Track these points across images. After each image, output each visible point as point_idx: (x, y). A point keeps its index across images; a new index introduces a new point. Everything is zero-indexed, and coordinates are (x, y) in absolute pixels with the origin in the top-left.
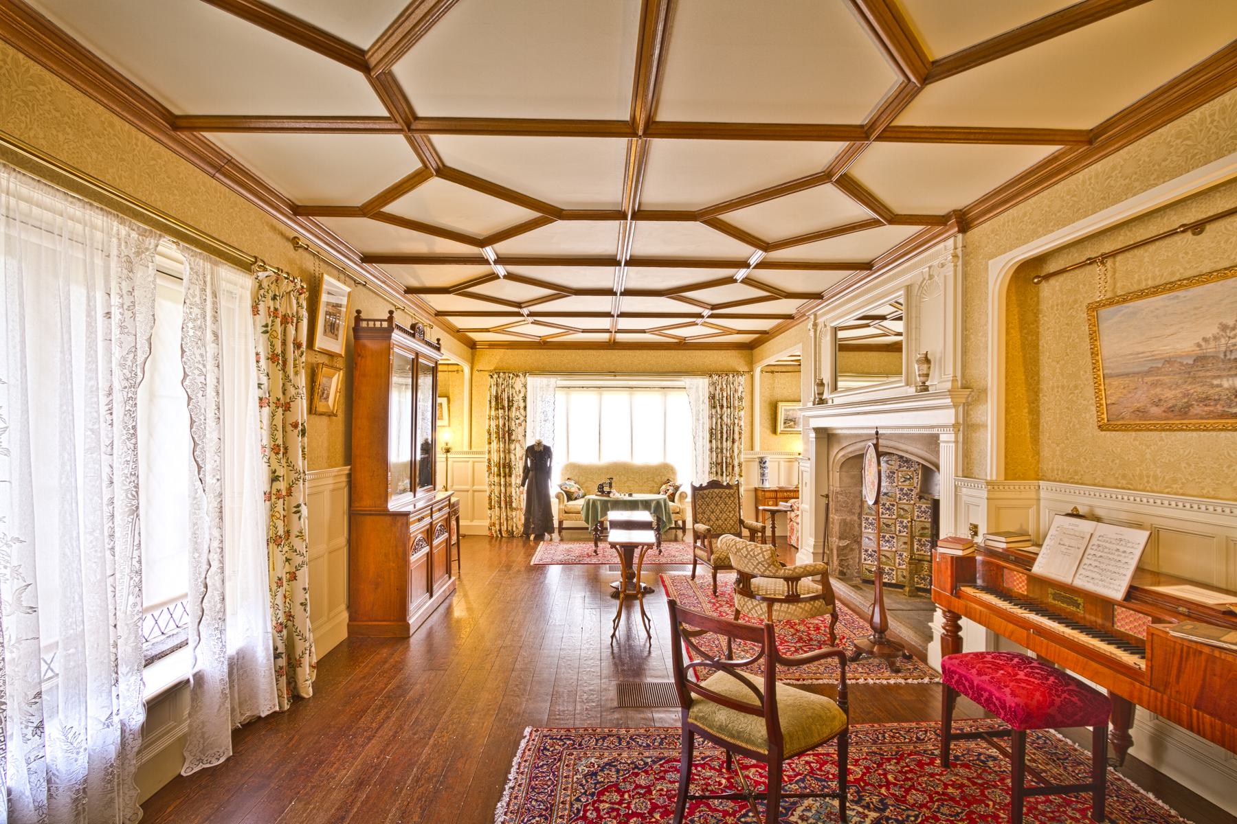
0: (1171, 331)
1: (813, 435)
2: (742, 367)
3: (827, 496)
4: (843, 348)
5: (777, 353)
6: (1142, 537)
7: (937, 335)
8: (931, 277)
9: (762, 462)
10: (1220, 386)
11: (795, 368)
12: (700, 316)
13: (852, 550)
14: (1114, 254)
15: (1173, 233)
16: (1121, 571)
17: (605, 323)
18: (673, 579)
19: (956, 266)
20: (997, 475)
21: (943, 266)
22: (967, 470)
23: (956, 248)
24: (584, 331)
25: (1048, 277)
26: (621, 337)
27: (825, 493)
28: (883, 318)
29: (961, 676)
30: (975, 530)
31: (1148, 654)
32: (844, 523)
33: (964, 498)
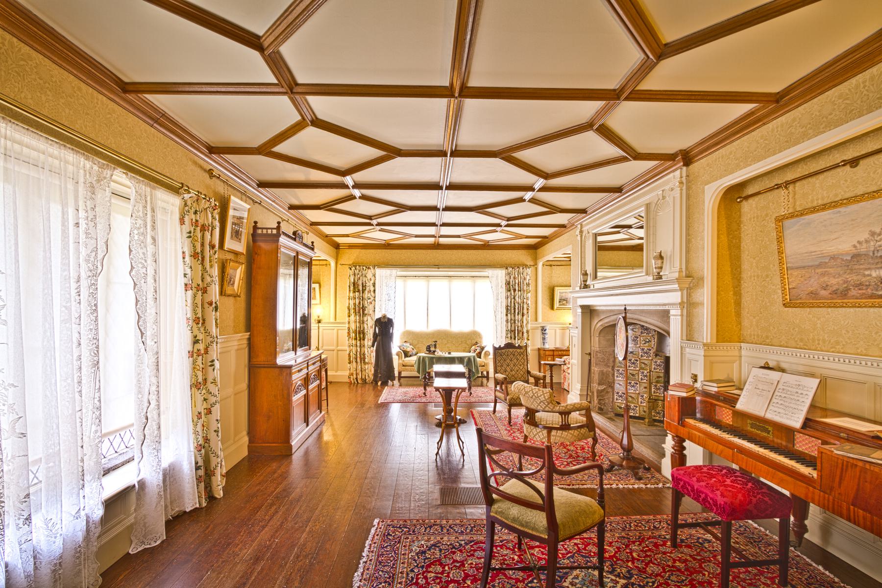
0: (835, 237)
1: (579, 310)
2: (529, 262)
3: (590, 354)
4: (601, 248)
5: (554, 252)
6: (814, 383)
7: (668, 239)
8: (664, 197)
9: (543, 330)
10: (870, 275)
11: (567, 262)
12: (499, 225)
13: (607, 392)
14: (794, 181)
15: (837, 166)
16: (800, 407)
17: (431, 230)
18: (480, 413)
19: (681, 190)
20: (711, 339)
21: (672, 189)
22: (689, 335)
23: (681, 177)
24: (417, 236)
25: (747, 197)
26: (443, 241)
27: (588, 352)
28: (630, 227)
29: (685, 482)
30: (695, 378)
31: (819, 467)
32: (602, 373)
33: (687, 355)
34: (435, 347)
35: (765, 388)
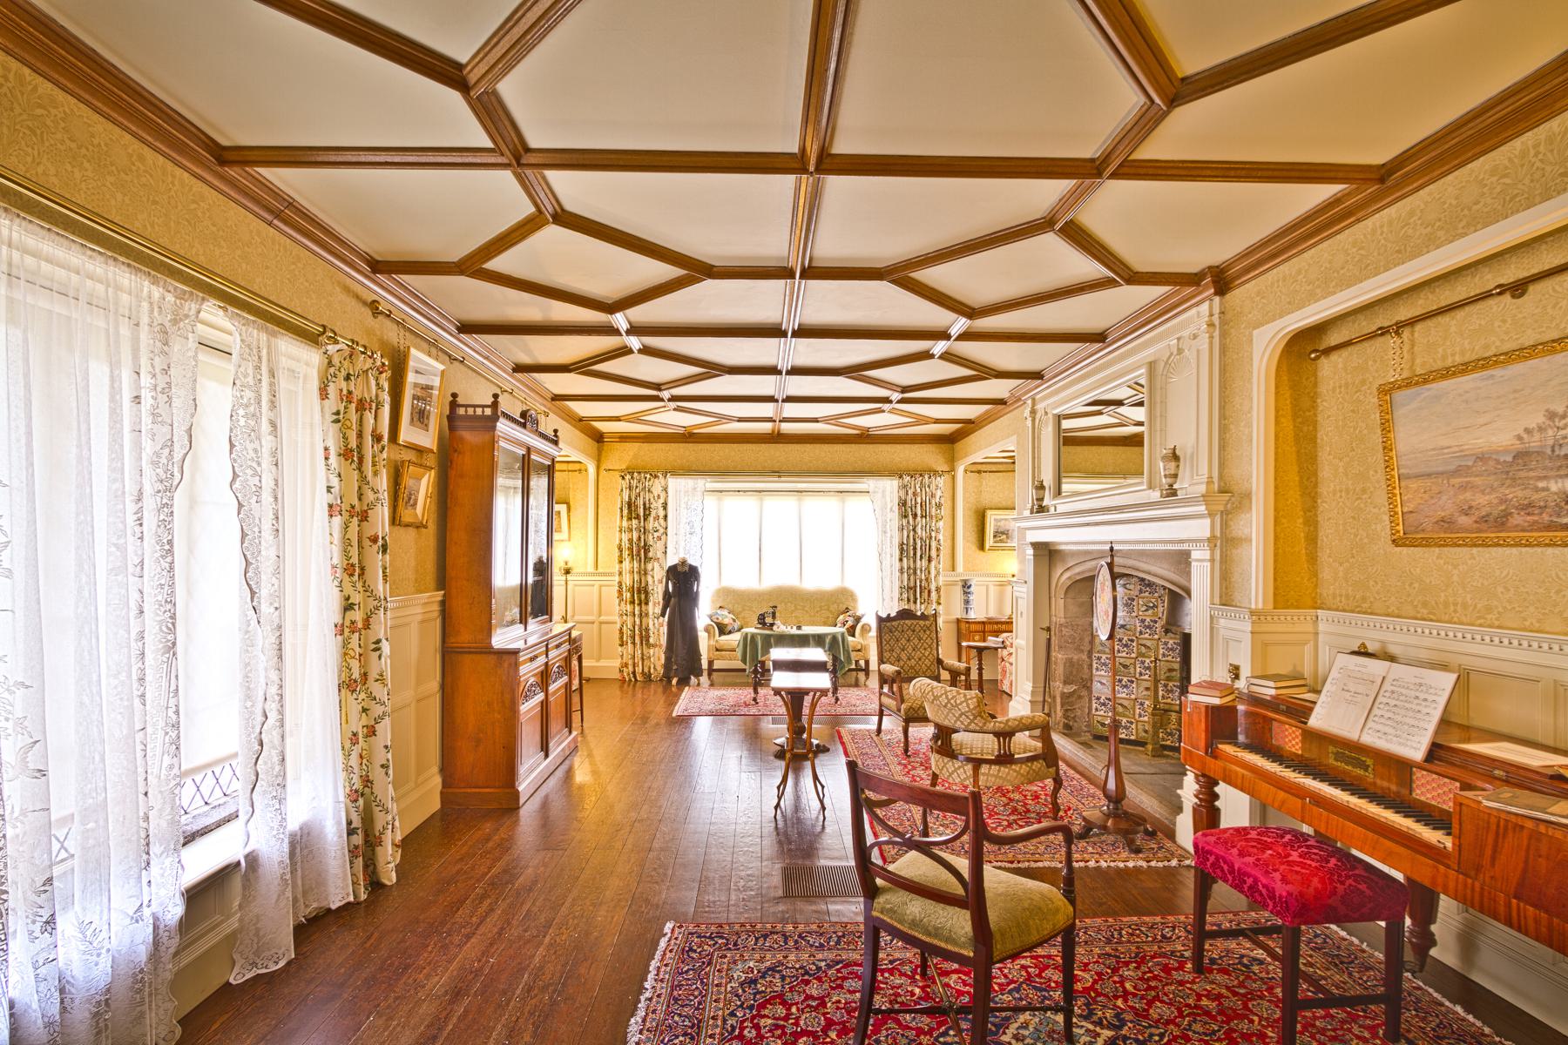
1: (1030, 551)
2: (941, 466)
3: (1049, 629)
4: (1068, 441)
5: (985, 447)
6: (1447, 680)
7: (1187, 424)
8: (1180, 351)
9: (966, 586)
10: (1546, 489)
12: (887, 400)
13: (1080, 697)
14: (1412, 322)
17: (766, 409)
18: (853, 734)
19: (1211, 337)
20: (1264, 602)
21: (1195, 337)
22: (1226, 596)
23: (1211, 315)
24: (741, 420)
25: (1328, 351)
26: (787, 428)
27: (1046, 625)
28: (1120, 403)
29: (1218, 857)
30: (1235, 672)
32: (1070, 663)
33: (1222, 632)
34: (774, 617)
35: (1361, 689)
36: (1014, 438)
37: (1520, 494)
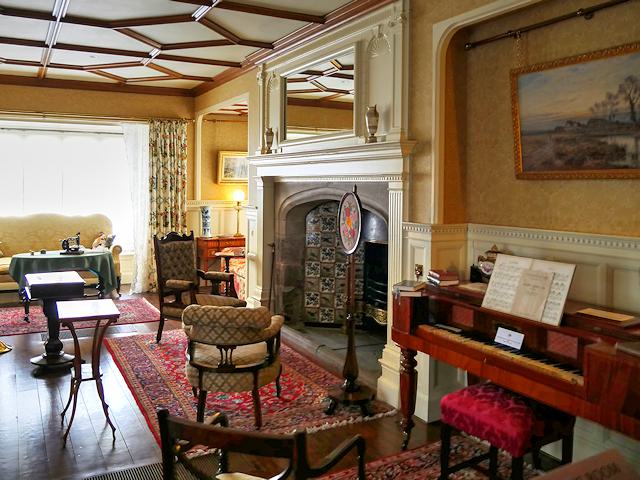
0: (564, 96)
1: (260, 183)
2: (185, 115)
3: (273, 245)
4: (290, 102)
5: (224, 101)
6: (567, 271)
7: (386, 92)
8: (381, 35)
9: (204, 211)
10: (604, 143)
11: (242, 116)
12: (147, 55)
13: (296, 295)
14: (527, 30)
15: (573, 15)
16: (557, 301)
17: (36, 54)
18: (120, 341)
19: (404, 27)
20: (439, 220)
21: (393, 25)
22: (412, 214)
23: (404, 11)
24: (8, 62)
25: (475, 45)
26: (52, 72)
27: (271, 242)
28: (320, 74)
29: (461, 415)
30: (420, 270)
31: (585, 373)
32: (289, 269)
33: (410, 242)
34: (78, 243)
35: (538, 283)
36: (247, 94)
37: (591, 146)
